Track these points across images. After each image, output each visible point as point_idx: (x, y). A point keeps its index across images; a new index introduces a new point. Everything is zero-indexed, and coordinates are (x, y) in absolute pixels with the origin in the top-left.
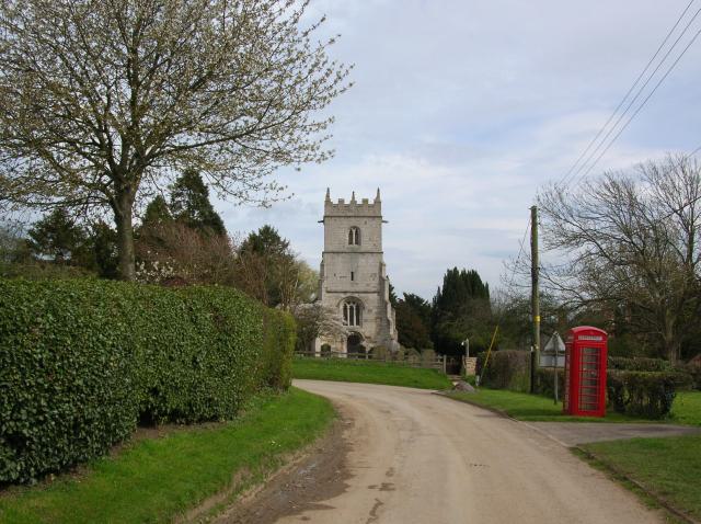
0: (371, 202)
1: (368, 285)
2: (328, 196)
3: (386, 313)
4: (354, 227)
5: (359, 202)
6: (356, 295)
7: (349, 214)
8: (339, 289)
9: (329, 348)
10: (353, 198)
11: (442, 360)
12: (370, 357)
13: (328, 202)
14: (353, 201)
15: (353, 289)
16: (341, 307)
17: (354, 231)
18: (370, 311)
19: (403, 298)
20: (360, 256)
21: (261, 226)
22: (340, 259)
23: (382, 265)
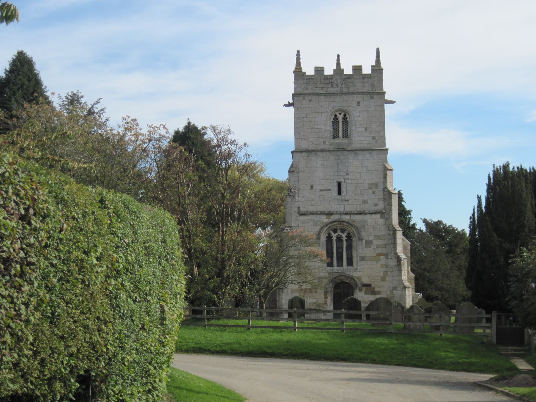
0: (367, 70)
1: (365, 202)
2: (298, 63)
3: (394, 244)
4: (341, 111)
5: (348, 71)
6: (346, 218)
7: (332, 90)
8: (320, 208)
9: (302, 303)
10: (338, 64)
11: (489, 320)
12: (368, 317)
13: (298, 72)
14: (339, 70)
15: (341, 209)
16: (323, 238)
17: (340, 117)
18: (369, 243)
19: (424, 228)
20: (351, 156)
21: (185, 124)
22: (318, 161)
23: (385, 171)
